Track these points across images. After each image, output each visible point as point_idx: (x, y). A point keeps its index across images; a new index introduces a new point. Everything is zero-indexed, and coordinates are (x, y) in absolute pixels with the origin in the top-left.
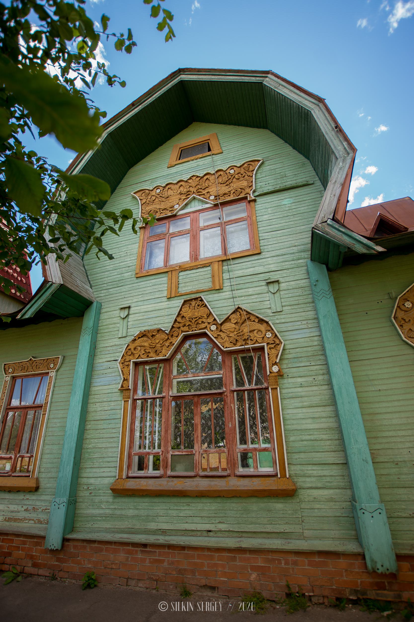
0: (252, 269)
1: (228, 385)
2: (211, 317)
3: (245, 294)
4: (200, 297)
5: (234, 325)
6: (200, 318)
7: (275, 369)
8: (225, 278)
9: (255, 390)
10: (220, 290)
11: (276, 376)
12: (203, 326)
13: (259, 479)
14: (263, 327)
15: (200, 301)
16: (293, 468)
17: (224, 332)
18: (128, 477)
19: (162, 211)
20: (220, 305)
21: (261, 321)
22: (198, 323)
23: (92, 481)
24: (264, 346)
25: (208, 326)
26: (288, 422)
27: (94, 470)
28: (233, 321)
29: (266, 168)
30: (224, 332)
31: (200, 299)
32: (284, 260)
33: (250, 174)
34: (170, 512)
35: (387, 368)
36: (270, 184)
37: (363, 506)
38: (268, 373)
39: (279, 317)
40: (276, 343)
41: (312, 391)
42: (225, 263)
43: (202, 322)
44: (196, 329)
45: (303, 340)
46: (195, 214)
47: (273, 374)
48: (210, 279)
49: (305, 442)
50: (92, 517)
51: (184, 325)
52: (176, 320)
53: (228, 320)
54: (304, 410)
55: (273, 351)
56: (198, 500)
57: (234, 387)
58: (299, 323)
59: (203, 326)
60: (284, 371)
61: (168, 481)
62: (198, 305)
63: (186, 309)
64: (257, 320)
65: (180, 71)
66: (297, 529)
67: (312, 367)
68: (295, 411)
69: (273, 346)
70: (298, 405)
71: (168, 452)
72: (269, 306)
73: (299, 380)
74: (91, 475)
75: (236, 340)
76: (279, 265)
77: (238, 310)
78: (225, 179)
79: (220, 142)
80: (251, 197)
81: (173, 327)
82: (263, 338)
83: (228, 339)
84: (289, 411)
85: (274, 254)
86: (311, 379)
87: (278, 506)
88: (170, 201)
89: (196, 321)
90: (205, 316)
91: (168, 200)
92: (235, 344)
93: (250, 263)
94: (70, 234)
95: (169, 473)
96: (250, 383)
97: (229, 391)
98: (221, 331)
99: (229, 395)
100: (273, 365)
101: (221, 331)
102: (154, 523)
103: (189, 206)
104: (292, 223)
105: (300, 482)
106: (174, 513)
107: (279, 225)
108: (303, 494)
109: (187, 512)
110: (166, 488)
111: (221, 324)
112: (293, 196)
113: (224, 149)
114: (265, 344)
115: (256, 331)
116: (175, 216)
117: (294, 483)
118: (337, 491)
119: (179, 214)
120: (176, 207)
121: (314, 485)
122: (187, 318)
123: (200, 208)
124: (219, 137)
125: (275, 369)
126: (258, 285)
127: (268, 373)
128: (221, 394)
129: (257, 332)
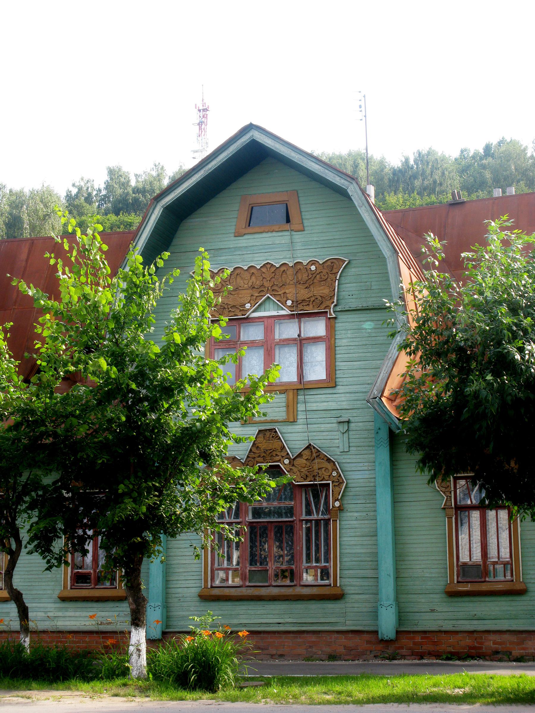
0: (325, 404)
1: (298, 514)
2: (284, 451)
3: (317, 429)
4: (275, 429)
5: (305, 461)
6: (274, 450)
7: (337, 504)
8: (299, 409)
9: (320, 520)
10: (294, 422)
11: (337, 510)
12: (277, 458)
13: (317, 587)
14: (329, 466)
15: (275, 432)
16: (343, 580)
17: (296, 467)
18: (212, 587)
19: (230, 309)
20: (295, 438)
21: (329, 460)
22: (272, 455)
23: (180, 590)
24: (329, 484)
25: (282, 459)
26: (343, 547)
27: (180, 582)
28: (305, 457)
29: (352, 271)
30: (296, 467)
31: (274, 431)
32: (356, 398)
33: (333, 276)
34: (249, 611)
35: (421, 510)
36: (354, 297)
37: (382, 603)
38: (331, 507)
39: (345, 457)
40: (339, 482)
41: (364, 524)
42: (301, 392)
43: (276, 455)
44: (271, 461)
45: (362, 480)
46: (270, 320)
47: (335, 509)
48: (285, 409)
49: (354, 563)
50: (182, 617)
51: (259, 456)
52: (251, 450)
53: (300, 455)
54: (356, 539)
55: (337, 489)
56: (271, 603)
57: (304, 517)
58: (361, 464)
59: (277, 458)
60: (345, 506)
61: (247, 590)
62: (273, 437)
63: (260, 439)
64: (325, 459)
65: (250, 127)
66: (342, 620)
67: (367, 504)
68: (350, 539)
69: (337, 484)
70: (352, 536)
71: (246, 568)
72: (337, 446)
73: (356, 514)
74: (178, 586)
75: (307, 476)
76: (352, 402)
77: (309, 447)
78: (305, 277)
79: (302, 210)
80: (331, 314)
81: (248, 457)
82: (330, 476)
83: (299, 474)
84: (345, 539)
85: (348, 391)
86: (364, 514)
87: (330, 606)
88: (240, 296)
89: (271, 453)
90: (279, 448)
91: (238, 294)
92: (305, 480)
93: (324, 396)
94: (264, 550)
95: (247, 584)
96: (318, 513)
97: (298, 520)
98: (293, 465)
99: (298, 523)
100: (336, 500)
101: (293, 465)
102: (236, 620)
103: (263, 308)
104: (369, 354)
105: (348, 590)
106: (252, 612)
107: (357, 355)
108: (350, 598)
109: (262, 611)
110: (246, 594)
111: (294, 459)
112: (374, 319)
113: (306, 223)
114: (330, 482)
115: (324, 469)
116: (247, 318)
117: (342, 590)
118: (371, 596)
119: (251, 316)
120: (248, 306)
121: (356, 592)
122: (261, 449)
123: (275, 313)
124: (301, 199)
125: (337, 504)
126: (329, 422)
127: (331, 507)
128: (293, 521)
129: (325, 470)
